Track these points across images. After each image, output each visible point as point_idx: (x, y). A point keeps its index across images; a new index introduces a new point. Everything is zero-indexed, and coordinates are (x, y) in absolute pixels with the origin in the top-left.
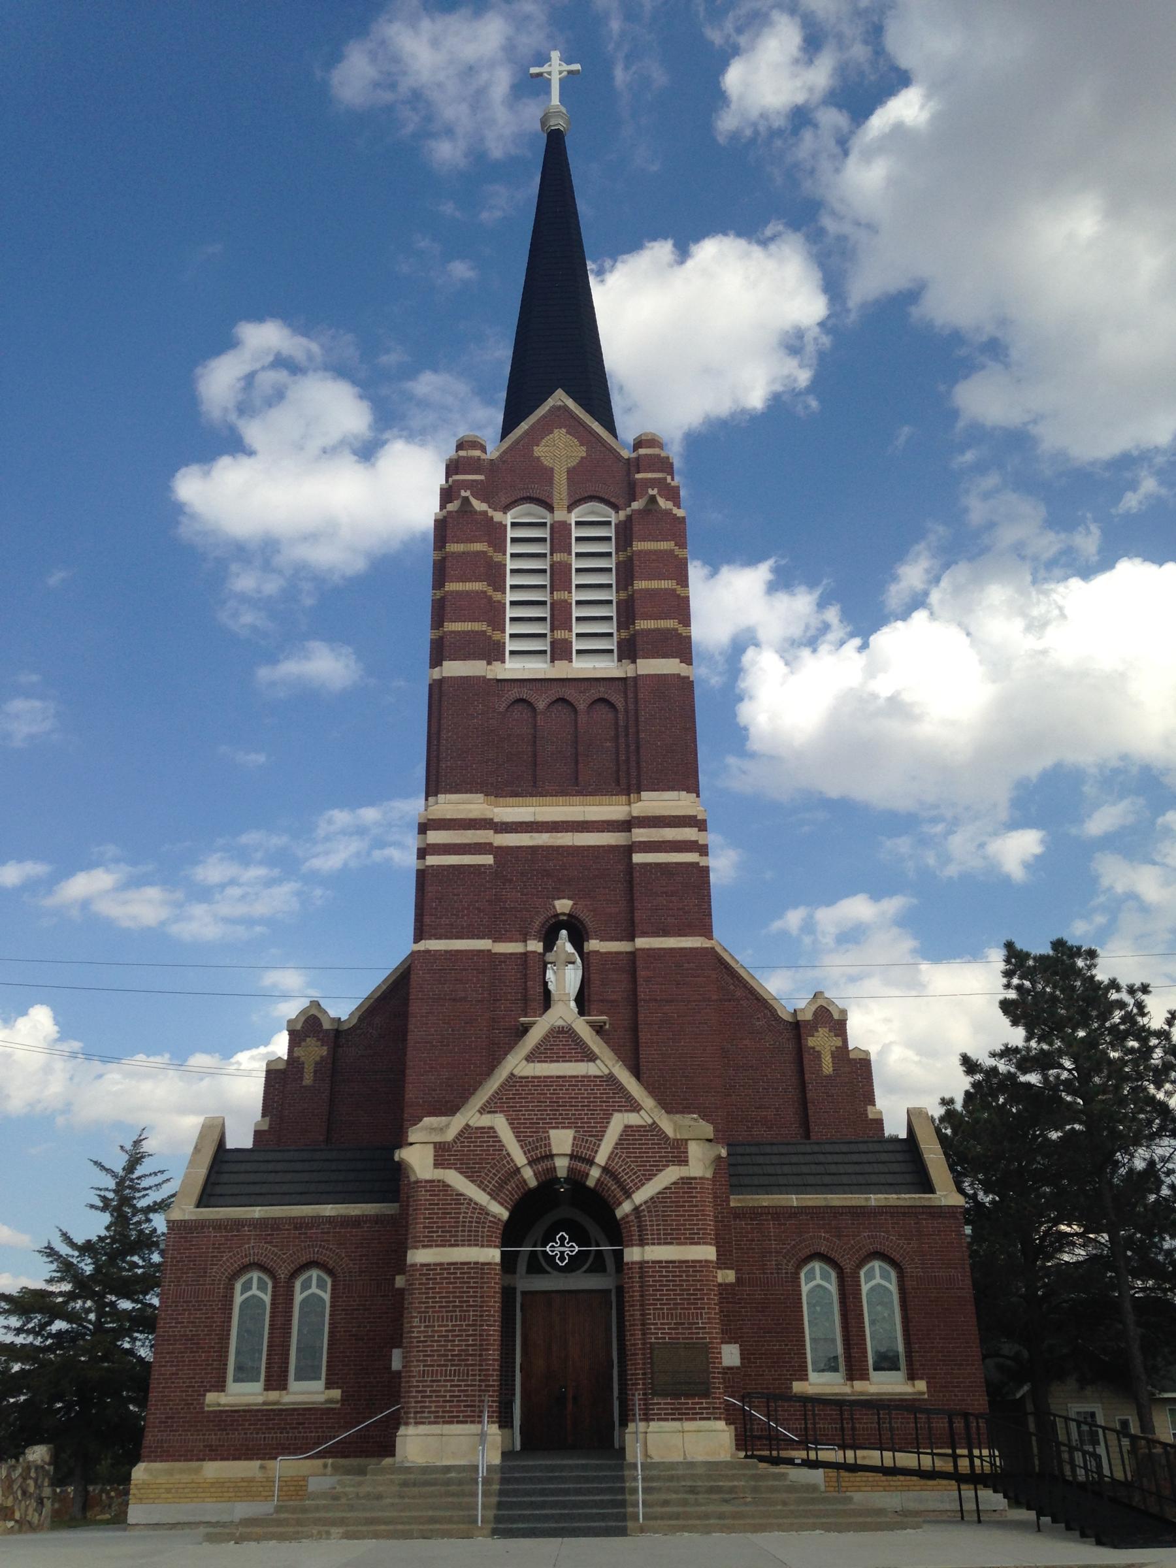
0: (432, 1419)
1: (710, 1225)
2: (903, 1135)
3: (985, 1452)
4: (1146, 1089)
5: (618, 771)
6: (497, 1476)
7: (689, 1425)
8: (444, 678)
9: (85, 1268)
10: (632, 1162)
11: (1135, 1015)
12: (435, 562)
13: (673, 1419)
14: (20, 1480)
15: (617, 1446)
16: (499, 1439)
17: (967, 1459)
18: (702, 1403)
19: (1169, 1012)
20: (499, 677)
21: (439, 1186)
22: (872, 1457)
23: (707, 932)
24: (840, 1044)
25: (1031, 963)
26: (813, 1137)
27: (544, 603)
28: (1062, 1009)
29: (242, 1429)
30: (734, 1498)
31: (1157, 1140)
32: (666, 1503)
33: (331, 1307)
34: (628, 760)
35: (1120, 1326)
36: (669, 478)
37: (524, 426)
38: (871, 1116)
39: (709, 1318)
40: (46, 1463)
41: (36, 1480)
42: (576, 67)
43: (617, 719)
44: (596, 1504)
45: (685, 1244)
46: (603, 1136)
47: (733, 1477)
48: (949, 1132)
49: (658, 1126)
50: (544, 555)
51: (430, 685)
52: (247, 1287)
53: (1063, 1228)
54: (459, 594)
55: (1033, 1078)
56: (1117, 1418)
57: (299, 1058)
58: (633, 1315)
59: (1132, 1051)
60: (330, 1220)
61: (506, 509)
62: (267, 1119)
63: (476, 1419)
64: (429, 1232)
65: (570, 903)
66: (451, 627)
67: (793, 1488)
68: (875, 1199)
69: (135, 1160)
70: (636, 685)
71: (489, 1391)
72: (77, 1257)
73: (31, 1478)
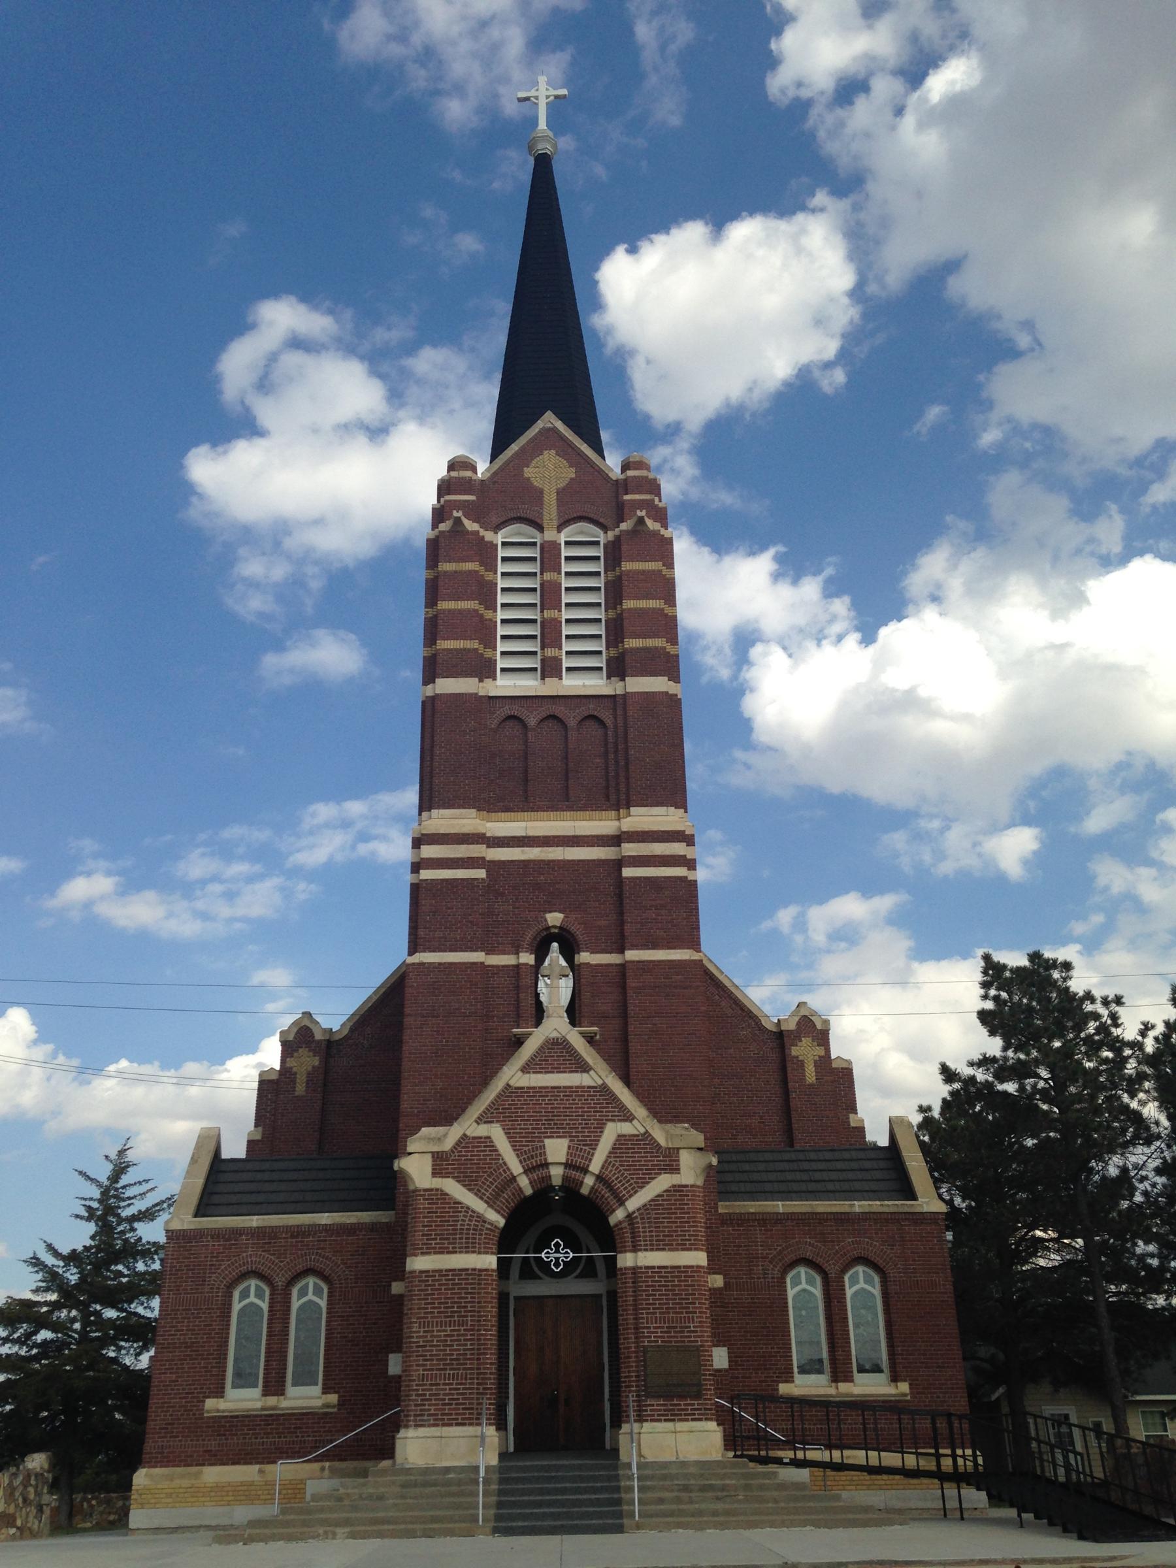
0: (432, 1422)
1: (701, 1231)
2: (884, 1142)
3: (969, 1452)
4: (1120, 1098)
5: (607, 787)
6: (495, 1477)
7: (681, 1426)
8: (437, 695)
9: (71, 1278)
10: (625, 1170)
11: (1109, 1026)
12: (427, 580)
13: (665, 1420)
14: (21, 1488)
15: (608, 1446)
16: (496, 1440)
17: (950, 1459)
18: (694, 1404)
19: (1143, 1023)
20: (491, 694)
21: (437, 1195)
22: (857, 1456)
23: (695, 944)
24: (823, 1053)
25: (1008, 974)
26: (797, 1147)
27: (534, 621)
28: (1038, 1019)
29: (241, 1434)
30: (727, 1496)
31: (1131, 1149)
32: (661, 1501)
33: (327, 1313)
34: (617, 776)
35: (1094, 1330)
36: (656, 500)
37: (514, 447)
38: (852, 1124)
39: (700, 1322)
40: (45, 1471)
41: (36, 1487)
42: (564, 92)
43: (606, 735)
44: (592, 1503)
45: (677, 1250)
46: (597, 1145)
47: (724, 1477)
48: (926, 1139)
49: (650, 1135)
50: (535, 574)
51: (423, 702)
52: (245, 1294)
53: (1039, 1233)
54: (451, 612)
55: (1010, 1087)
56: (1091, 1420)
57: (291, 1068)
58: (626, 1319)
59: (1106, 1061)
60: (327, 1229)
61: (497, 528)
62: (260, 1129)
63: (475, 1421)
64: (427, 1240)
65: (561, 916)
66: (444, 644)
67: (782, 1486)
68: (859, 1206)
69: (120, 1169)
70: (625, 703)
71: (486, 1394)
72: (63, 1267)
73: (31, 1485)
